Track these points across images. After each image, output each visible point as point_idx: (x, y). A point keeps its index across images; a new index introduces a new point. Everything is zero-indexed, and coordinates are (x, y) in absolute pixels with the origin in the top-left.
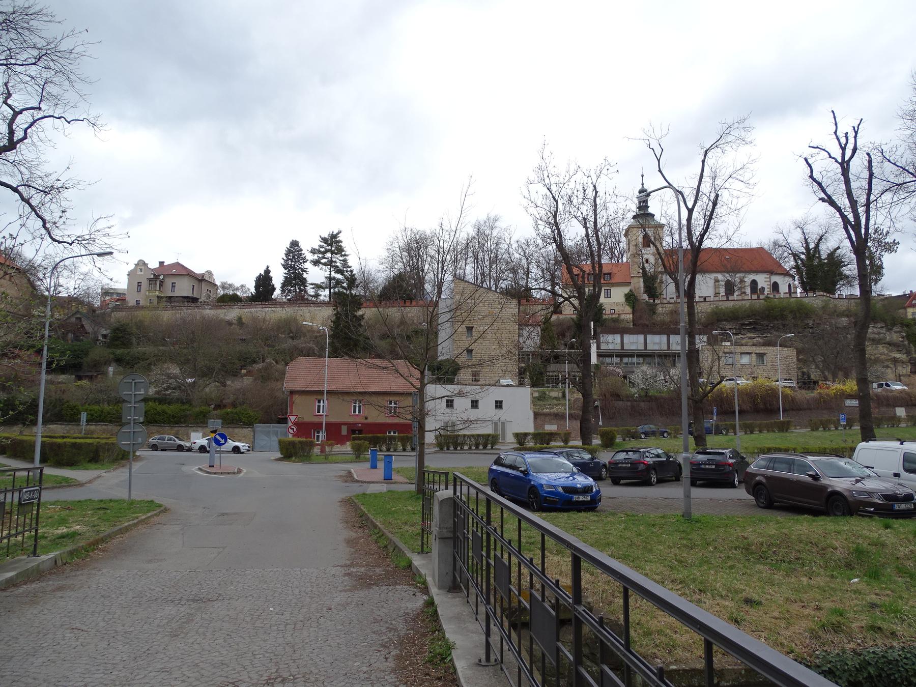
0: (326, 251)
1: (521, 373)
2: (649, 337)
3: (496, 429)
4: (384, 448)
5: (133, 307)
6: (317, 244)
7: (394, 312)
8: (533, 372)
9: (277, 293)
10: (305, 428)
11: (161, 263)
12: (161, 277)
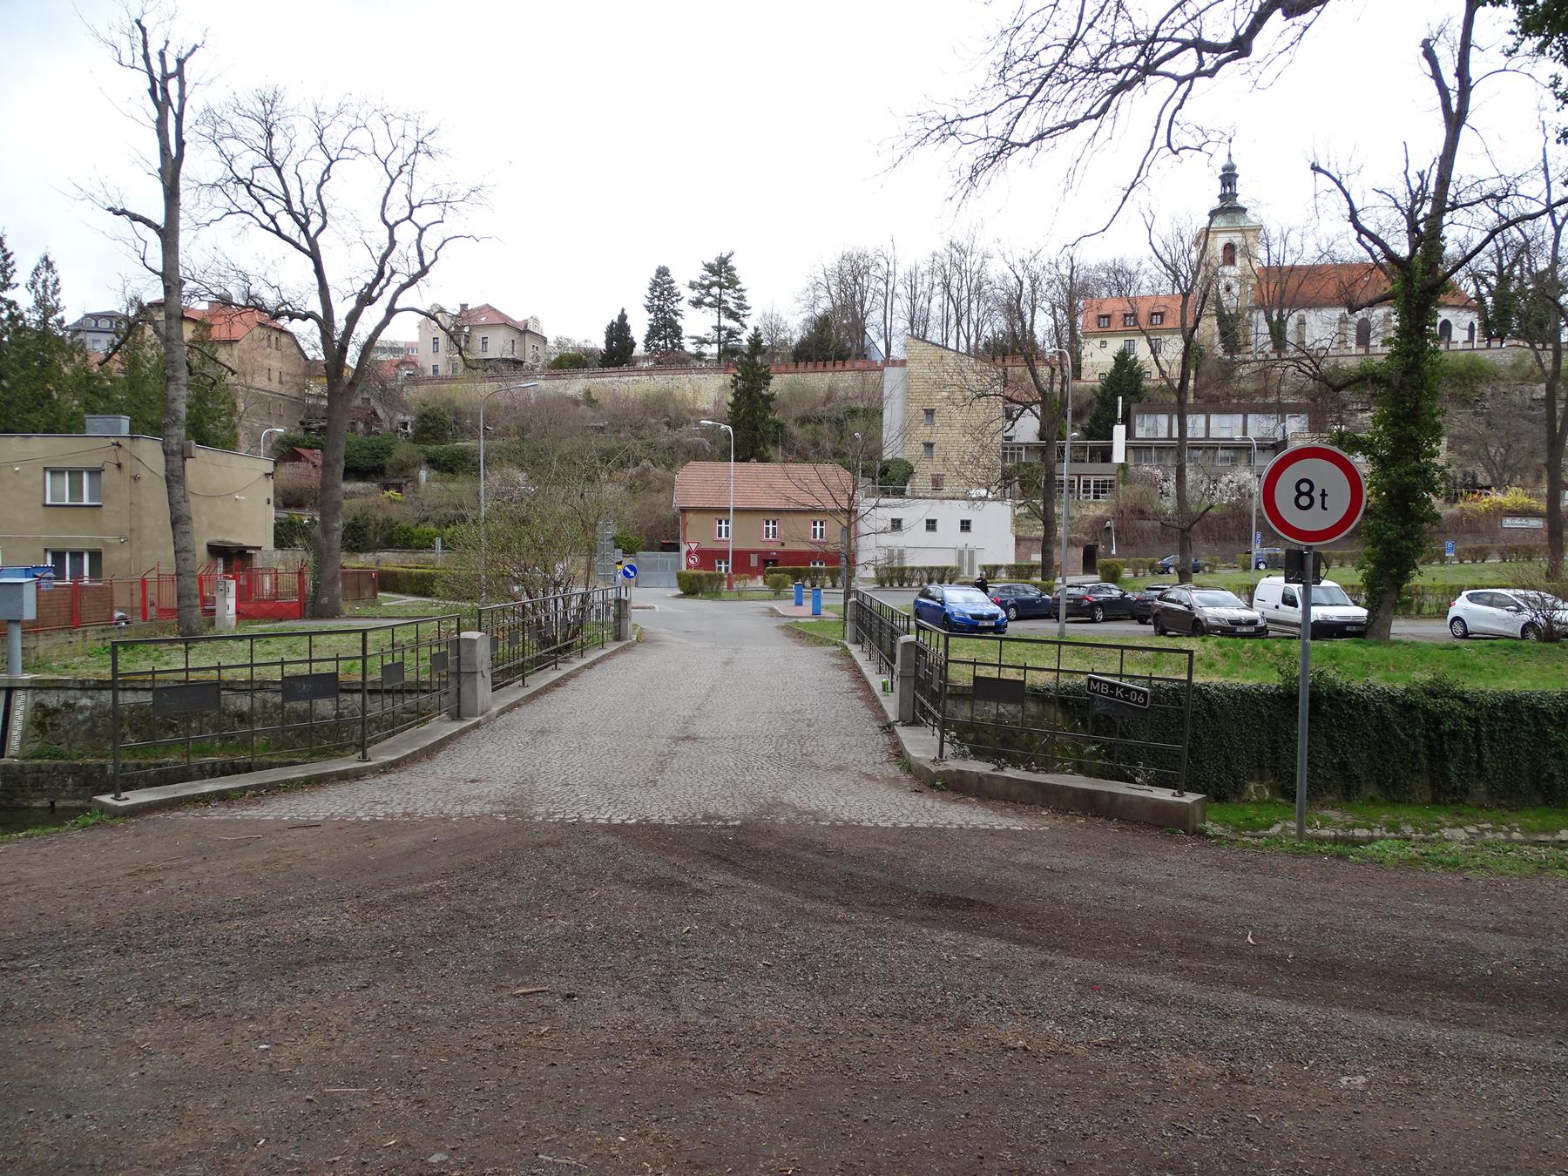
0: (712, 284)
1: (1007, 477)
2: (1214, 419)
3: (961, 560)
4: (808, 584)
5: (430, 379)
6: (697, 273)
7: (818, 381)
8: (1029, 479)
9: (639, 349)
10: (708, 557)
11: (464, 306)
12: (466, 329)
